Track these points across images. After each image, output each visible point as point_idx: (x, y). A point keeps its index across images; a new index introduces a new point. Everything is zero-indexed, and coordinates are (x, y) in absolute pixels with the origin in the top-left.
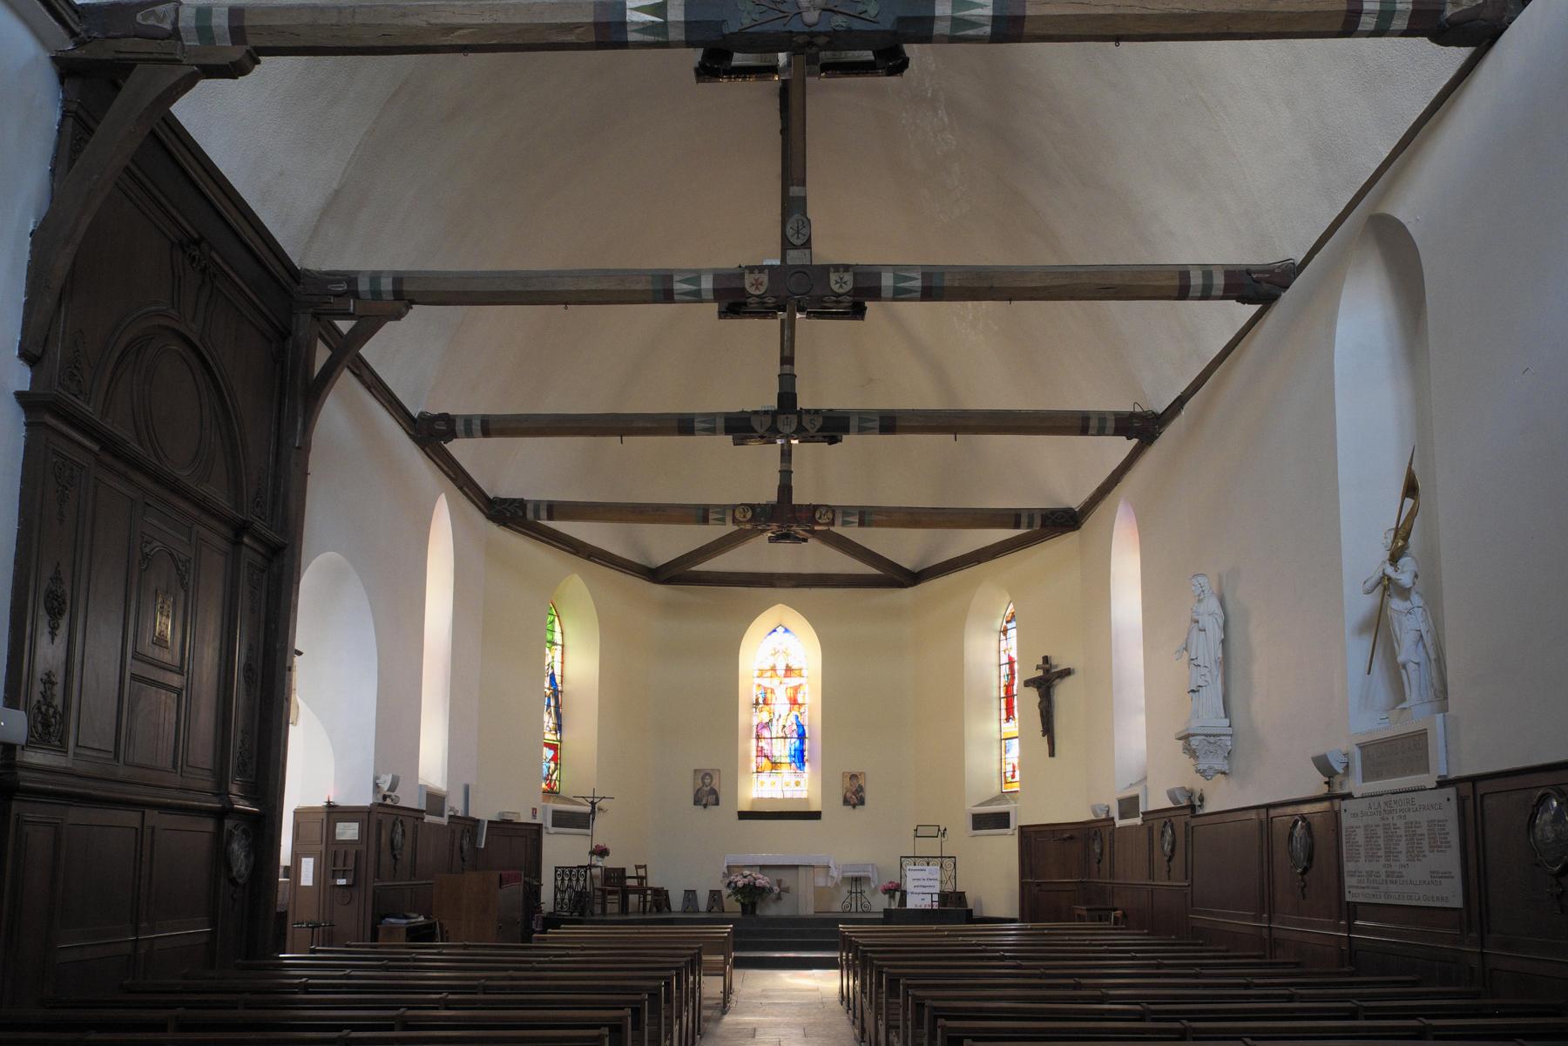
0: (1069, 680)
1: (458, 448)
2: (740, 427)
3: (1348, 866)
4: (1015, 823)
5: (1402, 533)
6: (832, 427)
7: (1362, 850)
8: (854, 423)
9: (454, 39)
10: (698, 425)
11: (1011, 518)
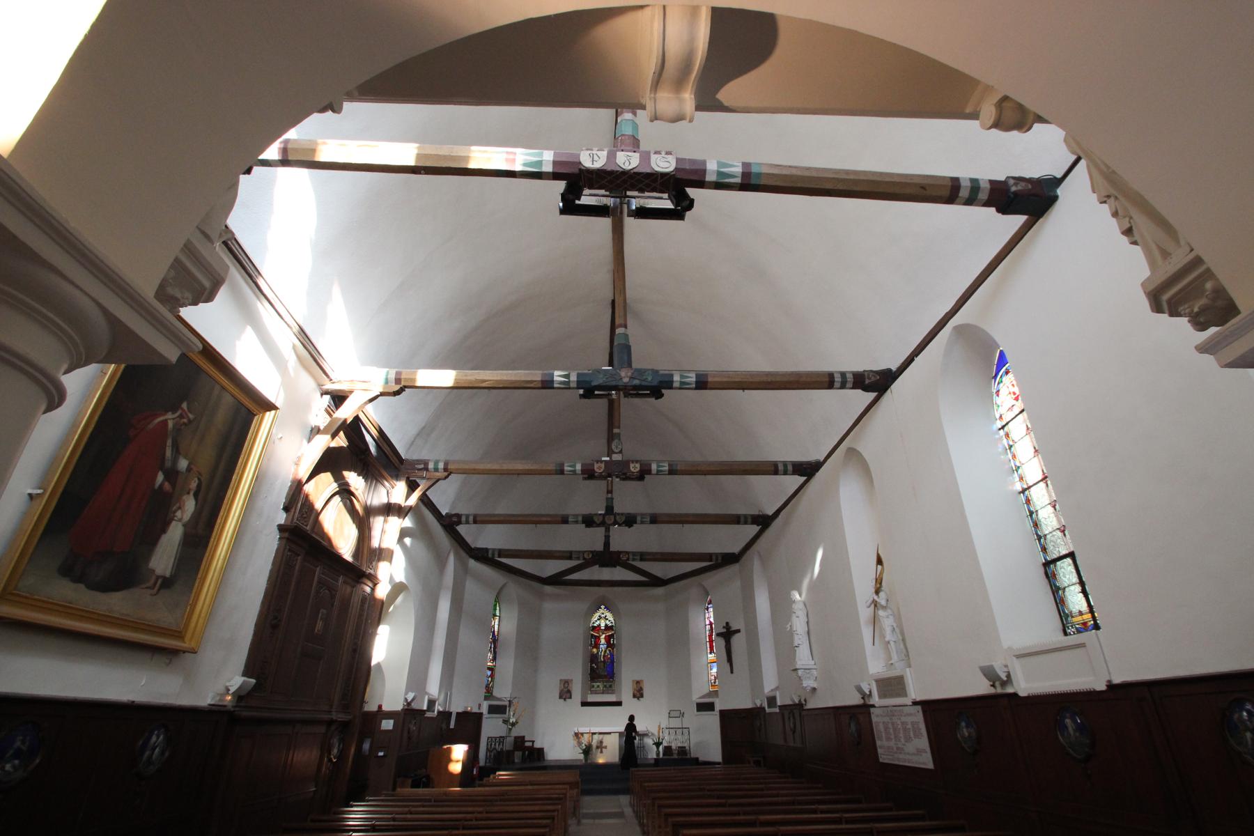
0: (737, 635)
1: (461, 529)
2: (589, 521)
3: (878, 743)
4: (718, 707)
5: (879, 582)
6: (630, 521)
8: (639, 519)
9: (484, 385)
11: (709, 557)
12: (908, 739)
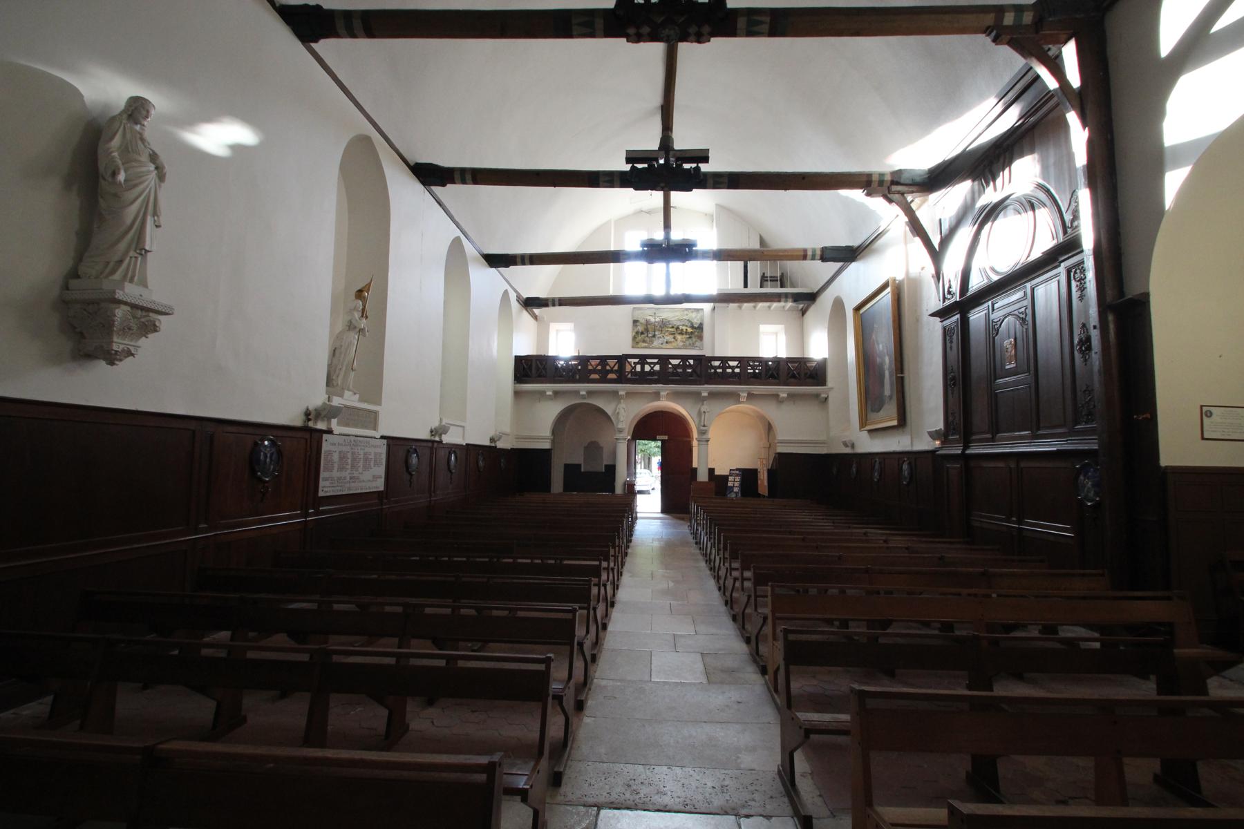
3: (323, 474)
7: (336, 465)
10: (726, 180)
12: (366, 468)
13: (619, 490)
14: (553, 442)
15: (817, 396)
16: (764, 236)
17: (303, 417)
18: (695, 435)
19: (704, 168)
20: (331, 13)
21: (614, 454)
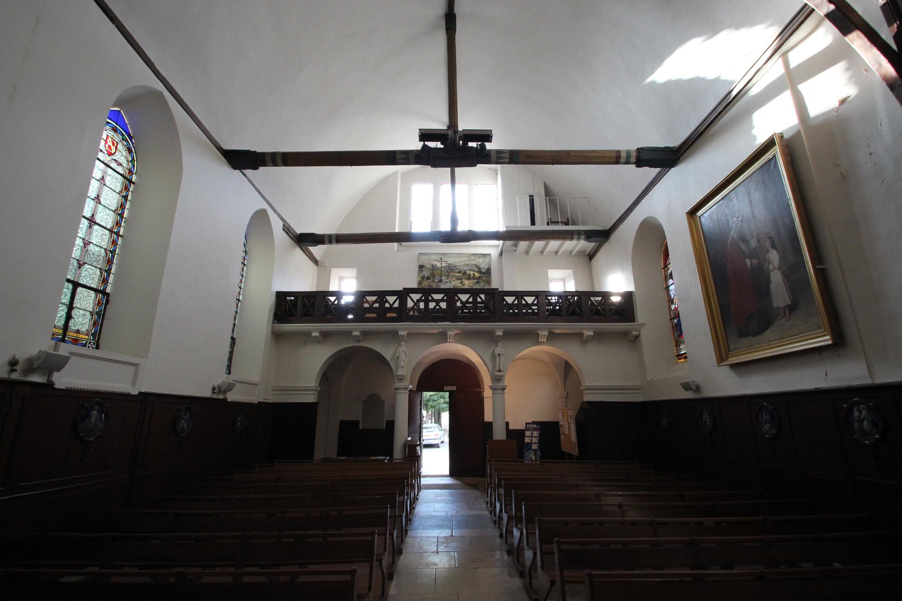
13: (398, 454)
14: (320, 394)
15: (625, 335)
16: (549, 183)
17: (8, 368)
18: (487, 381)
19: (489, 146)
20: (263, 154)
21: (393, 407)
